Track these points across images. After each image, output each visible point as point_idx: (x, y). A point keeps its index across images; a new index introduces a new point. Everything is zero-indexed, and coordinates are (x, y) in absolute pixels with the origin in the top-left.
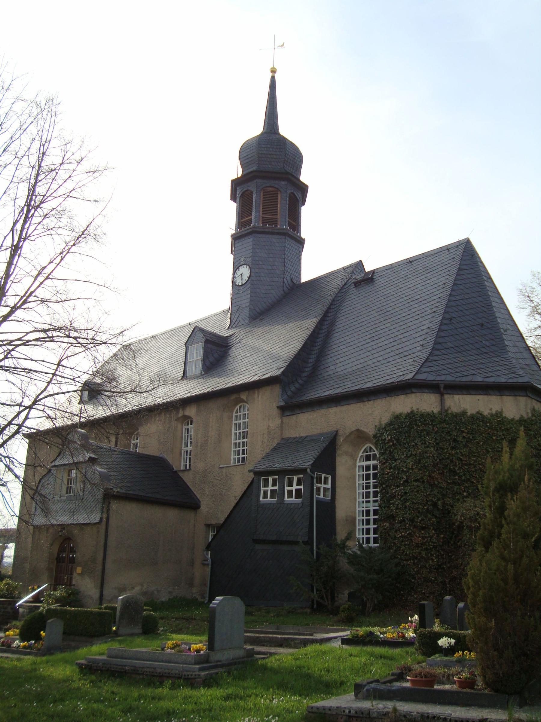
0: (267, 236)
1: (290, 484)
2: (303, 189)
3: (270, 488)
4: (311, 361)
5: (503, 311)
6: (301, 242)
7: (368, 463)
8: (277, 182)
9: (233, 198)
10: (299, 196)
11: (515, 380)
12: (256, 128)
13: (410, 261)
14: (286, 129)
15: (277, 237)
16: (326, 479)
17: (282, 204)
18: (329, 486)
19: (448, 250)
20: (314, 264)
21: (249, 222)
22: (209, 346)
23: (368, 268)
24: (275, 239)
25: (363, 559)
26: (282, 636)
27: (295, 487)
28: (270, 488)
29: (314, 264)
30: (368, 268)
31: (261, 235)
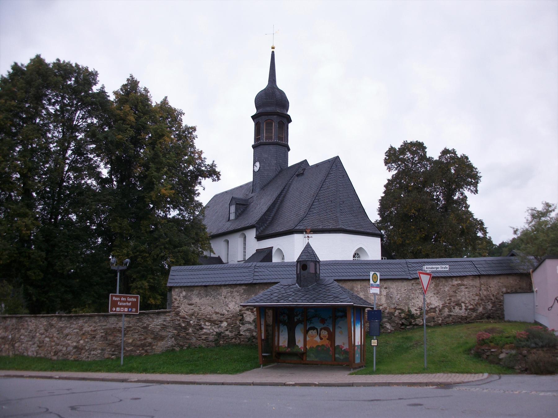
12: (264, 84)
14: (280, 84)
20: (293, 159)
23: (311, 163)
24: (271, 147)
29: (293, 159)
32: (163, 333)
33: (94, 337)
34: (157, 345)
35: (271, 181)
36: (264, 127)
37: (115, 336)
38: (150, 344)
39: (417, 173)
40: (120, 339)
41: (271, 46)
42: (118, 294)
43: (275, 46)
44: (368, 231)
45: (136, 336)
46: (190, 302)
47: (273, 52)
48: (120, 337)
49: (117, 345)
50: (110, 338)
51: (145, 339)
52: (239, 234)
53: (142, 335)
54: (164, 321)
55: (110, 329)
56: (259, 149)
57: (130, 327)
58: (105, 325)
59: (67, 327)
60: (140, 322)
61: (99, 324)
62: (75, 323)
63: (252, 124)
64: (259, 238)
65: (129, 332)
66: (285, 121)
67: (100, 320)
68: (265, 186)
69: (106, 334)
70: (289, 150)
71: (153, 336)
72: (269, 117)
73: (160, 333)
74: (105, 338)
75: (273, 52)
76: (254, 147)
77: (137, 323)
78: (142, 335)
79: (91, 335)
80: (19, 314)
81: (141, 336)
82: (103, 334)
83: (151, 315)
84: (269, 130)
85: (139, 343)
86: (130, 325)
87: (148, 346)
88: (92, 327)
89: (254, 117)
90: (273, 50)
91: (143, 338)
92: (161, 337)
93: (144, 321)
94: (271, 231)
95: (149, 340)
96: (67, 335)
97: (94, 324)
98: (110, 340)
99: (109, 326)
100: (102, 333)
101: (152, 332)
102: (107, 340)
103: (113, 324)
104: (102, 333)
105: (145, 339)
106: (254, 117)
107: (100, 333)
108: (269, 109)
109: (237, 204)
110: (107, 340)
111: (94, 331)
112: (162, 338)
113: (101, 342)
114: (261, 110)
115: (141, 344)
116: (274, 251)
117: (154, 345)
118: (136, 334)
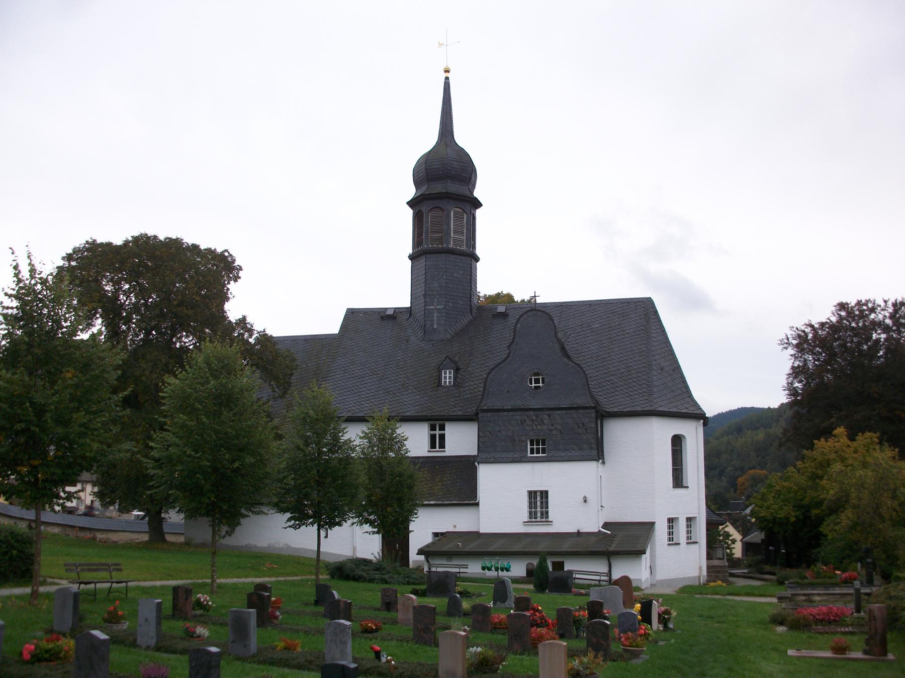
12: (429, 140)
14: (461, 138)
36: (428, 219)
39: (371, 458)
42: (437, 449)
44: (639, 409)
46: (385, 586)
47: (447, 78)
48: (197, 383)
56: (422, 260)
63: (409, 212)
66: (468, 207)
70: (477, 259)
75: (447, 78)
76: (411, 257)
80: (18, 597)
89: (411, 204)
106: (411, 204)
108: (438, 188)
114: (423, 189)
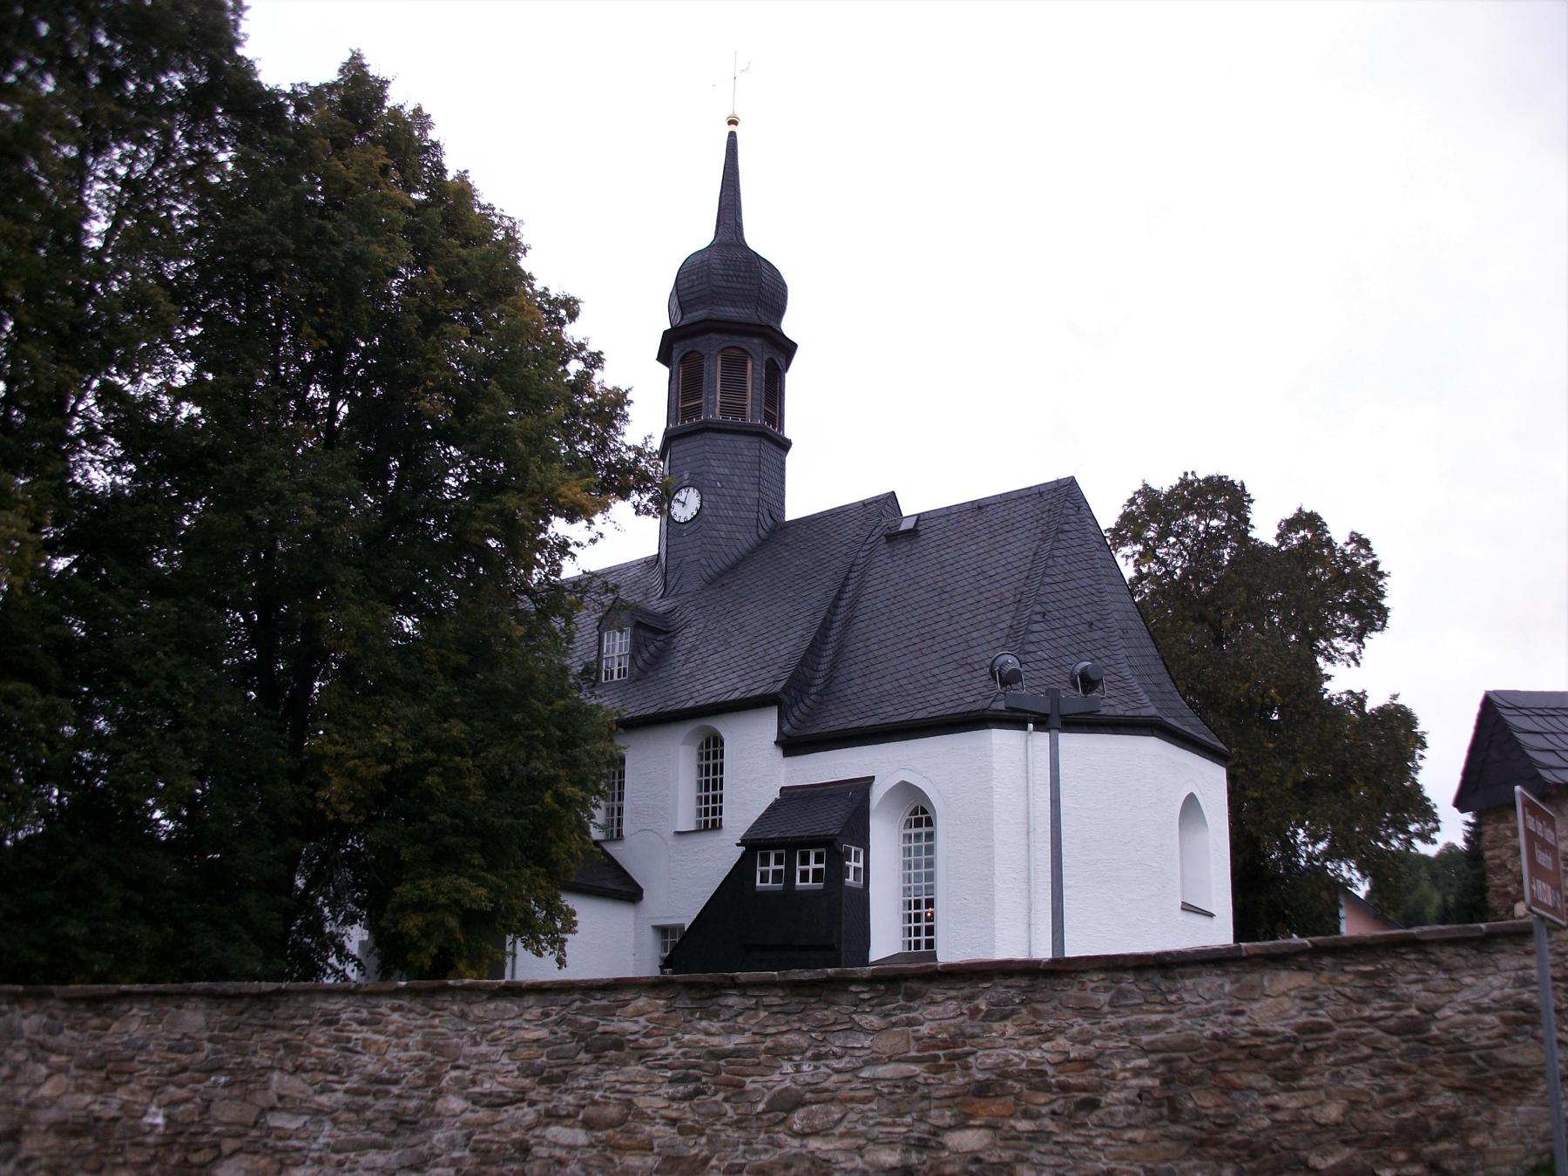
0: (728, 437)
1: (805, 861)
2: (788, 349)
3: (772, 866)
4: (823, 667)
5: (1114, 580)
6: (785, 445)
7: (918, 830)
8: (745, 339)
9: (664, 356)
10: (780, 362)
11: (1136, 713)
12: (703, 234)
13: (979, 507)
14: (758, 237)
15: (745, 438)
16: (857, 854)
17: (753, 374)
18: (861, 865)
19: (1040, 494)
20: (809, 490)
21: (697, 410)
22: (641, 632)
23: (911, 506)
24: (742, 443)
25: (558, 897)
26: (1154, 1037)
27: (812, 865)
28: (772, 866)
29: (809, 490)
30: (911, 506)
31: (717, 436)
32: (1522, 1055)
33: (1092, 1105)
34: (1492, 1125)
35: (741, 561)
36: (715, 370)
37: (1229, 1088)
38: (1453, 1124)
40: (1263, 1106)
41: (727, 113)
43: (740, 115)
45: (1361, 1080)
47: (732, 135)
49: (1245, 1145)
50: (1205, 1101)
51: (1417, 1095)
52: (685, 730)
53: (1398, 1070)
54: (1524, 982)
55: (1190, 1045)
57: (1326, 1028)
58: (1157, 1027)
59: (777, 1053)
60: (1383, 993)
61: (1114, 1021)
62: (873, 1020)
64: (791, 745)
65: (1322, 1060)
67: (1121, 994)
68: (722, 574)
69: (1166, 1082)
71: (1460, 1075)
72: (737, 341)
73: (1505, 1055)
74: (1163, 1106)
75: (732, 135)
77: (1363, 1002)
78: (1398, 1070)
79: (1065, 1088)
81: (1389, 1080)
82: (1148, 1082)
83: (1444, 955)
84: (734, 383)
85: (1385, 1120)
86: (1323, 1017)
87: (1444, 1135)
88: (1061, 1042)
90: (733, 128)
91: (1402, 1087)
92: (1513, 1076)
93: (1403, 989)
94: (835, 722)
95: (1443, 1100)
96: (787, 1103)
97: (1080, 1024)
98: (1198, 1115)
99: (1178, 1027)
100: (1138, 1072)
101: (1457, 1050)
102: (1175, 1115)
103: (1206, 1014)
104: (1138, 1072)
105: (1417, 1095)
107: (1130, 1077)
109: (638, 625)
110: (1175, 1115)
111: (1087, 1063)
112: (1518, 1082)
113: (1139, 1135)
115: (1401, 1128)
116: (877, 794)
117: (1476, 1128)
118: (1361, 1071)
